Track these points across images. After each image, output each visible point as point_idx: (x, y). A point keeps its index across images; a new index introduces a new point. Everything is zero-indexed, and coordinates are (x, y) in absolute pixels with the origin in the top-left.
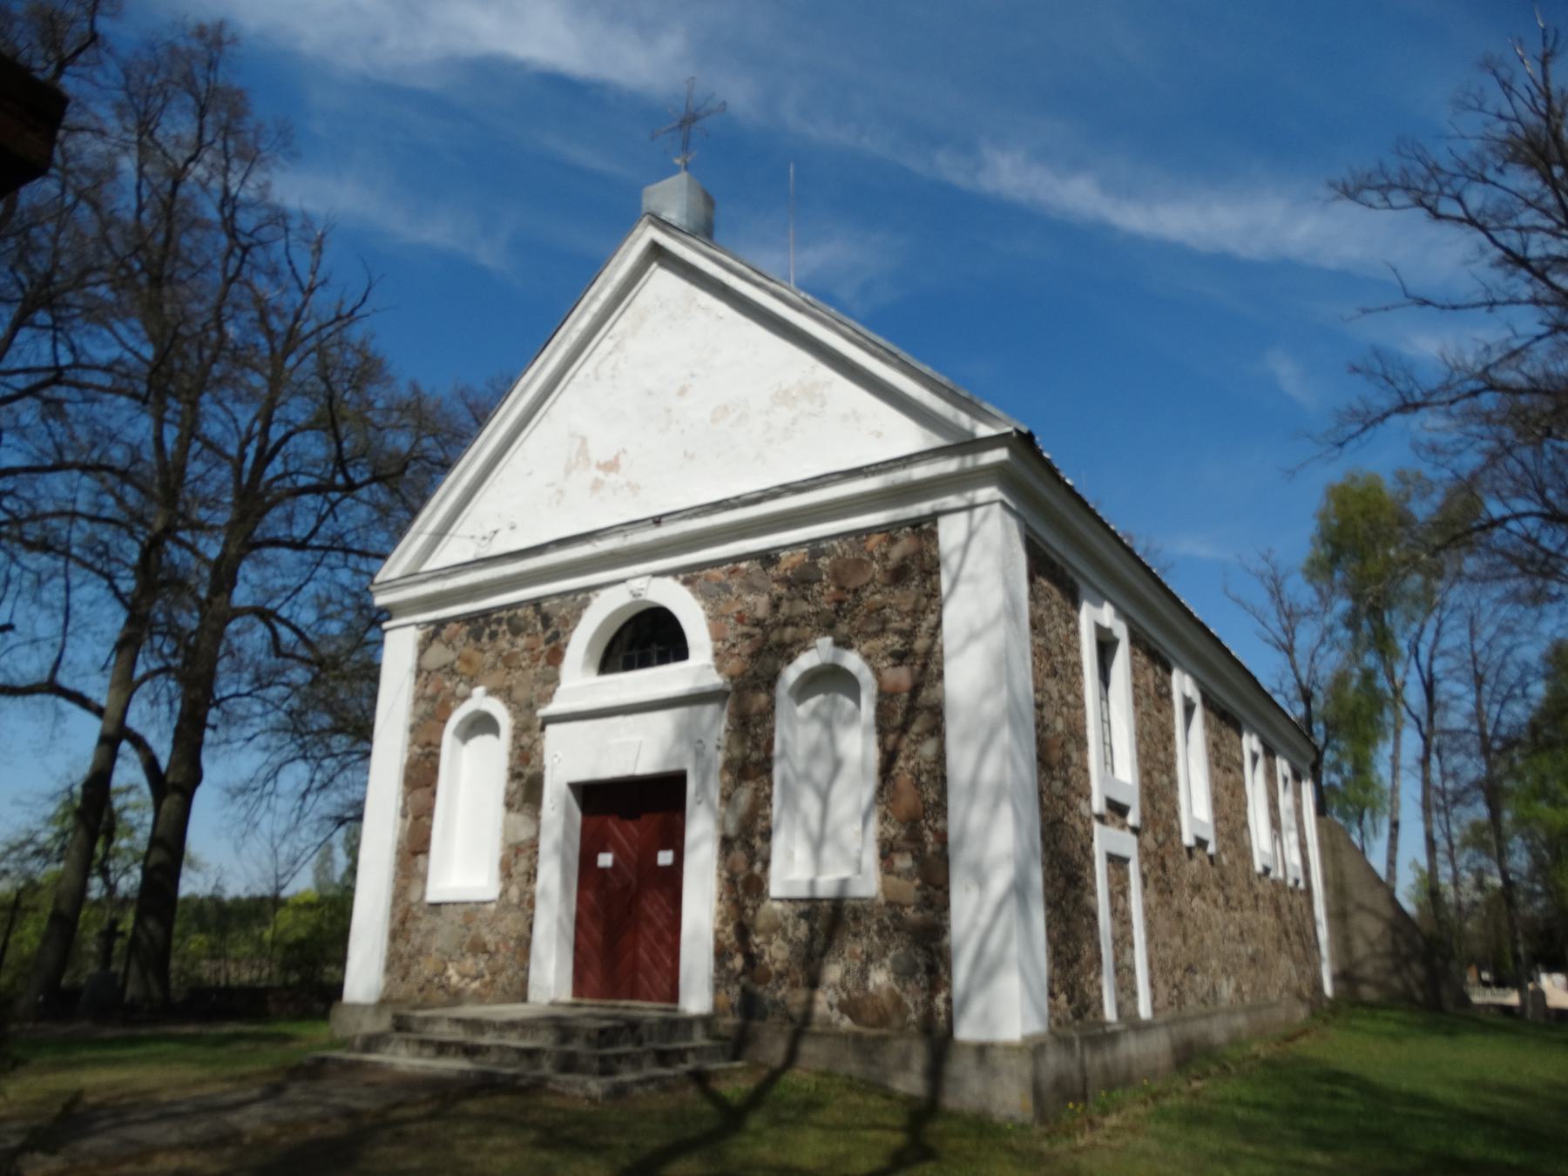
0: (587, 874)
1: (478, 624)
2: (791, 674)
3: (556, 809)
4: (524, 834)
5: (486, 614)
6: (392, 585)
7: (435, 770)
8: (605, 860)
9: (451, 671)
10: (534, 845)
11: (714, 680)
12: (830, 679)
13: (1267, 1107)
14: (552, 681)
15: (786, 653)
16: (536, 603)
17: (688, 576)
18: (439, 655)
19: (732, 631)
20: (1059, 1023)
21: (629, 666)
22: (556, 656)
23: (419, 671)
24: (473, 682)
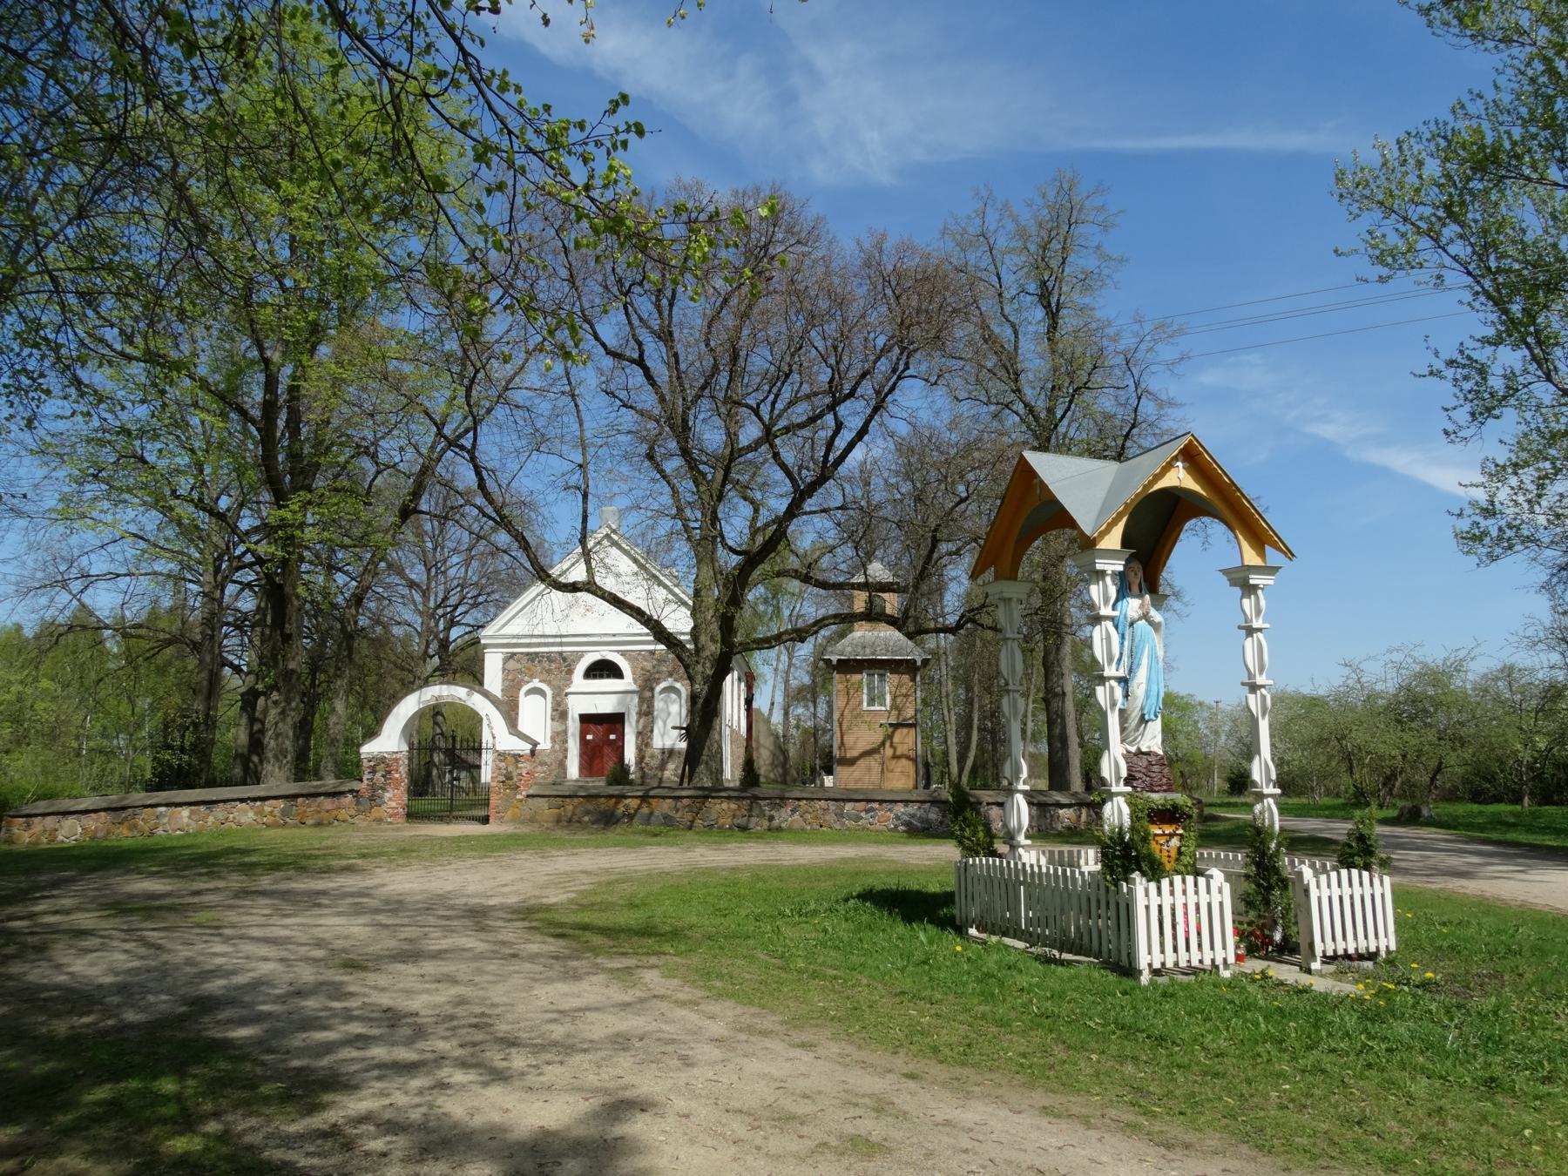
0: (584, 742)
1: (532, 657)
2: (658, 689)
3: (573, 726)
4: (560, 729)
5: (537, 654)
6: (486, 637)
7: (517, 706)
8: (589, 737)
9: (520, 672)
10: (565, 732)
11: (634, 687)
12: (671, 689)
13: (1159, 889)
14: (569, 681)
15: (658, 681)
16: (561, 653)
17: (623, 653)
18: (512, 664)
19: (639, 672)
20: (736, 216)
21: (595, 677)
22: (570, 672)
23: (504, 669)
24: (532, 677)
